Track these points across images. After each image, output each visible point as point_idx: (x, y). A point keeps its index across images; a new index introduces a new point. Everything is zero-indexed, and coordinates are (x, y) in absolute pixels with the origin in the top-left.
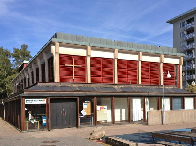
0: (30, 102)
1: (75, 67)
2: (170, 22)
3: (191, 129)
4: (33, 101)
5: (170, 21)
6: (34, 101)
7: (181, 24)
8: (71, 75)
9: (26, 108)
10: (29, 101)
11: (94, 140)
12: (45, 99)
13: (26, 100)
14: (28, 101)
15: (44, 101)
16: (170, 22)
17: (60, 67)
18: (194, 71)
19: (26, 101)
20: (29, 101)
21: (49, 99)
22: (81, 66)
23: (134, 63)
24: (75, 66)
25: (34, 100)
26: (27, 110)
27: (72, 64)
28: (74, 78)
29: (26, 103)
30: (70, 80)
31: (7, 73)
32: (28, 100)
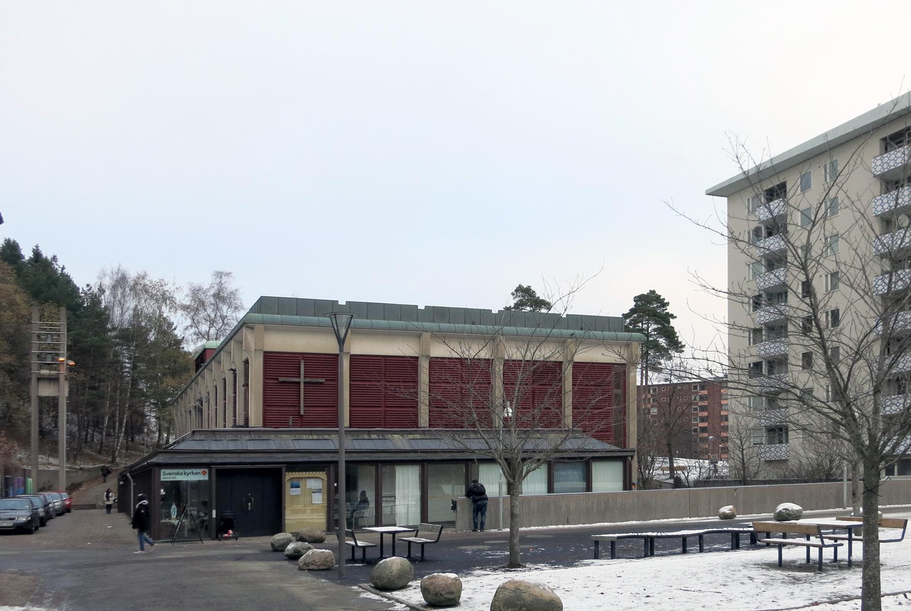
0: (172, 476)
1: (305, 383)
2: (716, 192)
3: (698, 537)
4: (178, 474)
5: (716, 191)
6: (182, 474)
7: (749, 199)
8: (334, 406)
9: (162, 491)
10: (170, 474)
11: (717, 592)
12: (207, 470)
13: (162, 471)
14: (167, 476)
15: (204, 473)
16: (716, 192)
17: (265, 385)
18: (58, 399)
19: (162, 474)
20: (170, 474)
21: (214, 471)
22: (323, 380)
23: (411, 363)
24: (308, 380)
25: (180, 471)
26: (164, 493)
27: (299, 377)
28: (302, 413)
29: (162, 480)
30: (291, 417)
31: (591, 397)
32: (167, 471)
